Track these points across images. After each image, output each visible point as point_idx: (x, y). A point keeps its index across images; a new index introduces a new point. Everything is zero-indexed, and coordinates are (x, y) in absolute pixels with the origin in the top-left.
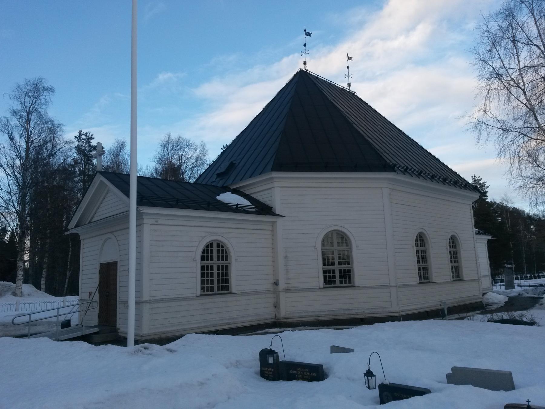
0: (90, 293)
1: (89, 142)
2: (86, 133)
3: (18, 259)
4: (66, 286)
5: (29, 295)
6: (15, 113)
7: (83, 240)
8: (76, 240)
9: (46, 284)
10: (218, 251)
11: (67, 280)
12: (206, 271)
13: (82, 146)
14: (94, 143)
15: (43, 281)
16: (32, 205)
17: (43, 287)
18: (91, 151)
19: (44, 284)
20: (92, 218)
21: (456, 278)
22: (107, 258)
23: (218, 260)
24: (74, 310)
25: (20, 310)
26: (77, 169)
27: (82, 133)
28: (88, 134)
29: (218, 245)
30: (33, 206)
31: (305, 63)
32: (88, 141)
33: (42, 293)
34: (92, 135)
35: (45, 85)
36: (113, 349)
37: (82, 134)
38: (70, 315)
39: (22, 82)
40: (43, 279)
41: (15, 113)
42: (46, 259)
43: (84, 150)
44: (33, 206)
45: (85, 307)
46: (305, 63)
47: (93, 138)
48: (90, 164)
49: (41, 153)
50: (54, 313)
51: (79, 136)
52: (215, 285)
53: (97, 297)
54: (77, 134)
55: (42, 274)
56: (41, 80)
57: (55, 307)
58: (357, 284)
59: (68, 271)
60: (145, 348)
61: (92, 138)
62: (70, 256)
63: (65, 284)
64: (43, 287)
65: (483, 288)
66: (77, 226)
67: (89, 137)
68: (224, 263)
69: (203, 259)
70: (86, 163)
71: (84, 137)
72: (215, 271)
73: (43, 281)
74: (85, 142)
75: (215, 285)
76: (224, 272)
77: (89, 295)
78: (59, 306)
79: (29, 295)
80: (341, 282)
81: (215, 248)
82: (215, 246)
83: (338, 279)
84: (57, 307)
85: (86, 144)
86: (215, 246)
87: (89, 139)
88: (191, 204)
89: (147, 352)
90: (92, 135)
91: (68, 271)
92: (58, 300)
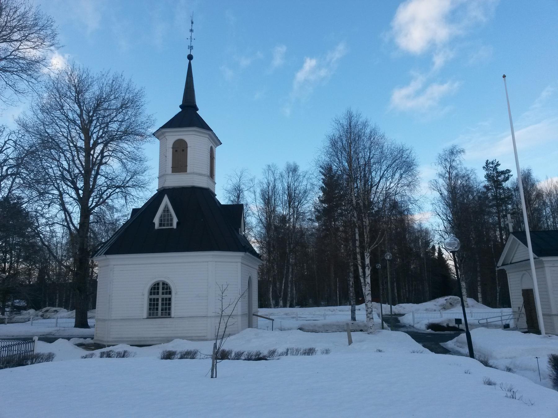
0: (519, 308)
1: (496, 169)
2: (492, 162)
3: (461, 280)
4: (498, 299)
5: (472, 306)
6: (440, 175)
7: (509, 273)
8: (503, 275)
9: (482, 298)
11: (498, 294)
13: (491, 173)
14: (500, 169)
15: (480, 295)
17: (480, 300)
18: (500, 176)
19: (481, 298)
20: (512, 260)
22: (526, 287)
24: (511, 318)
25: (474, 317)
26: (489, 194)
27: (489, 162)
28: (495, 162)
32: (495, 169)
33: (480, 305)
34: (498, 162)
35: (457, 149)
36: (533, 336)
37: (489, 163)
38: (508, 321)
39: (442, 152)
40: (479, 294)
41: (440, 175)
42: (479, 277)
43: (493, 176)
45: (517, 316)
47: (499, 165)
48: (500, 188)
50: (499, 319)
51: (487, 166)
53: (523, 310)
54: (484, 164)
55: (477, 290)
56: (454, 147)
57: (485, 318)
59: (498, 286)
60: (549, 336)
61: (498, 165)
62: (497, 273)
63: (496, 297)
64: (480, 300)
65: (393, 313)
66: (503, 265)
67: (496, 164)
68: (168, 296)
70: (497, 188)
71: (491, 165)
72: (160, 302)
73: (480, 295)
74: (492, 169)
76: (168, 303)
77: (518, 309)
78: (488, 317)
79: (472, 306)
81: (161, 286)
84: (486, 318)
85: (493, 170)
87: (496, 166)
89: (550, 338)
90: (498, 162)
91: (498, 286)
92: (497, 311)
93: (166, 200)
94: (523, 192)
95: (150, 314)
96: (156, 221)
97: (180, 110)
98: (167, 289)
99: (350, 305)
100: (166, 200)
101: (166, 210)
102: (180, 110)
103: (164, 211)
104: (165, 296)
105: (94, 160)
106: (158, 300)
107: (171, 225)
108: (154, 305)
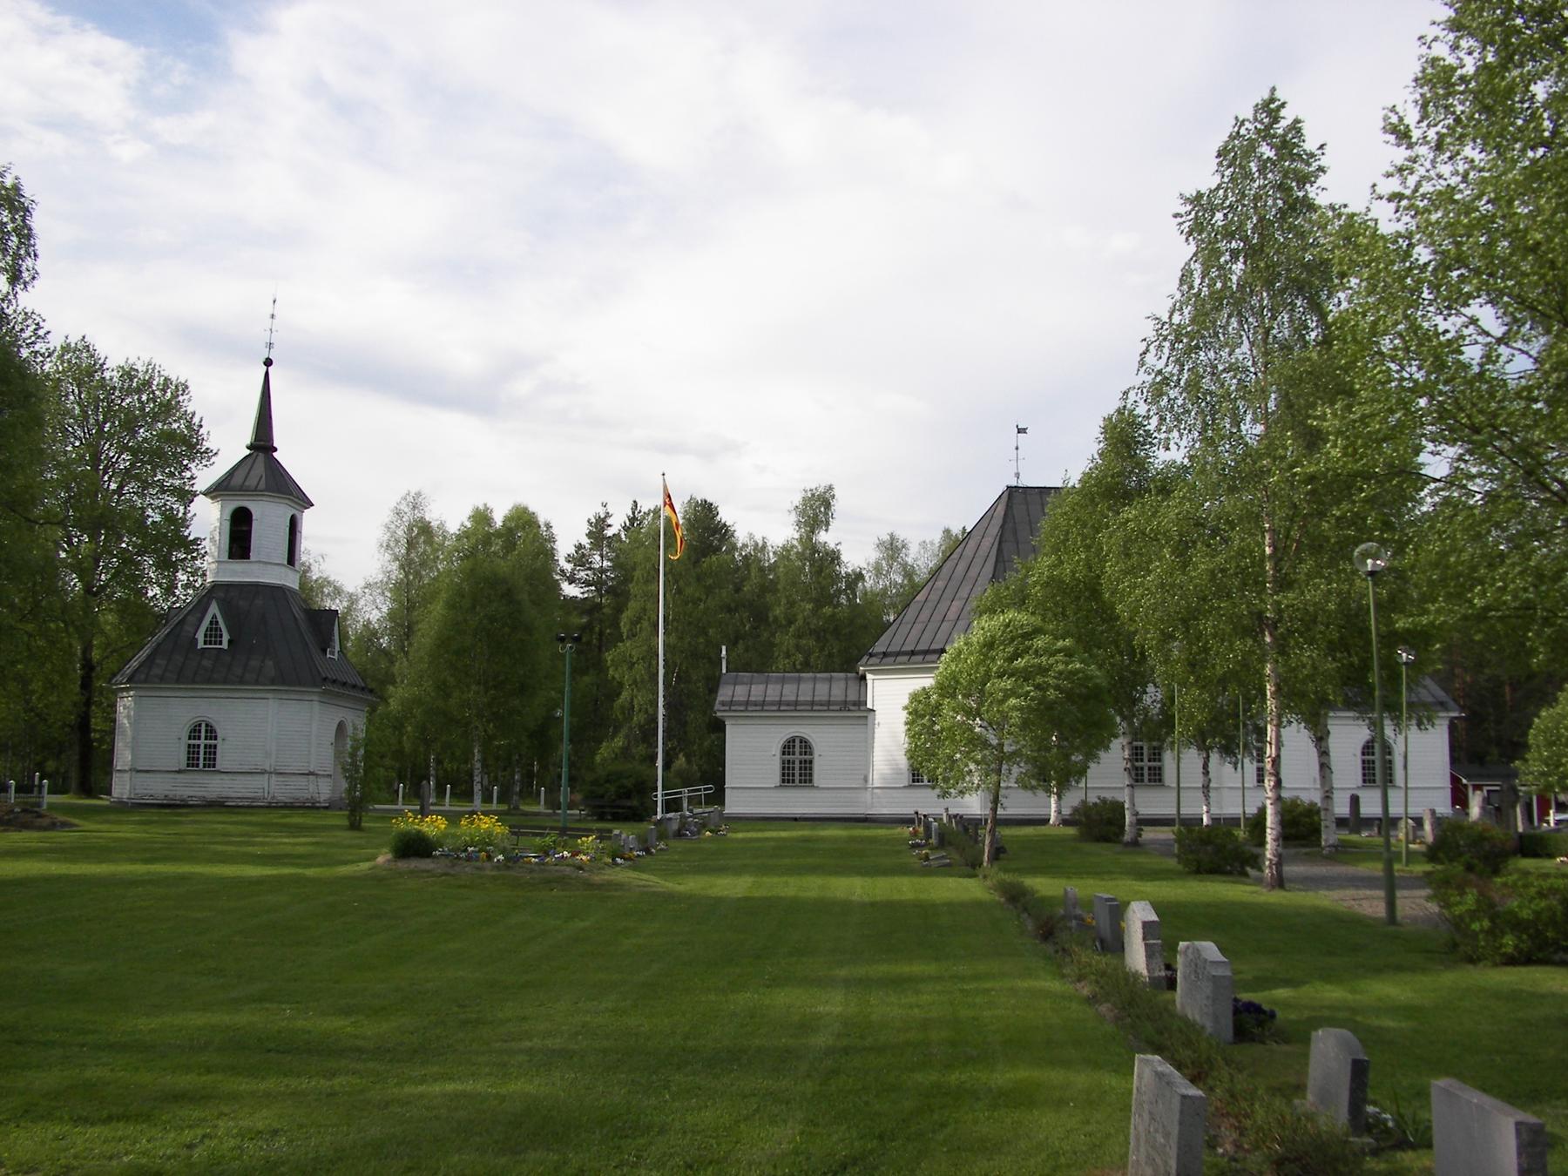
10: (206, 731)
12: (192, 752)
16: (1438, 649)
21: (1373, 754)
23: (801, 754)
29: (207, 725)
30: (1438, 646)
31: (1017, 475)
44: (1438, 646)
46: (1017, 475)
49: (400, 708)
52: (797, 777)
58: (1167, 784)
68: (807, 757)
69: (1363, 754)
72: (797, 765)
75: (797, 777)
76: (211, 751)
80: (1150, 780)
82: (797, 741)
83: (1146, 777)
86: (797, 741)
88: (233, 848)
93: (214, 609)
94: (25, 834)
95: (783, 781)
96: (200, 636)
97: (248, 452)
98: (211, 733)
99: (1306, 1041)
100: (214, 609)
101: (214, 622)
102: (248, 452)
103: (211, 623)
104: (791, 757)
105: (1555, 499)
106: (199, 746)
107: (221, 643)
108: (806, 769)
